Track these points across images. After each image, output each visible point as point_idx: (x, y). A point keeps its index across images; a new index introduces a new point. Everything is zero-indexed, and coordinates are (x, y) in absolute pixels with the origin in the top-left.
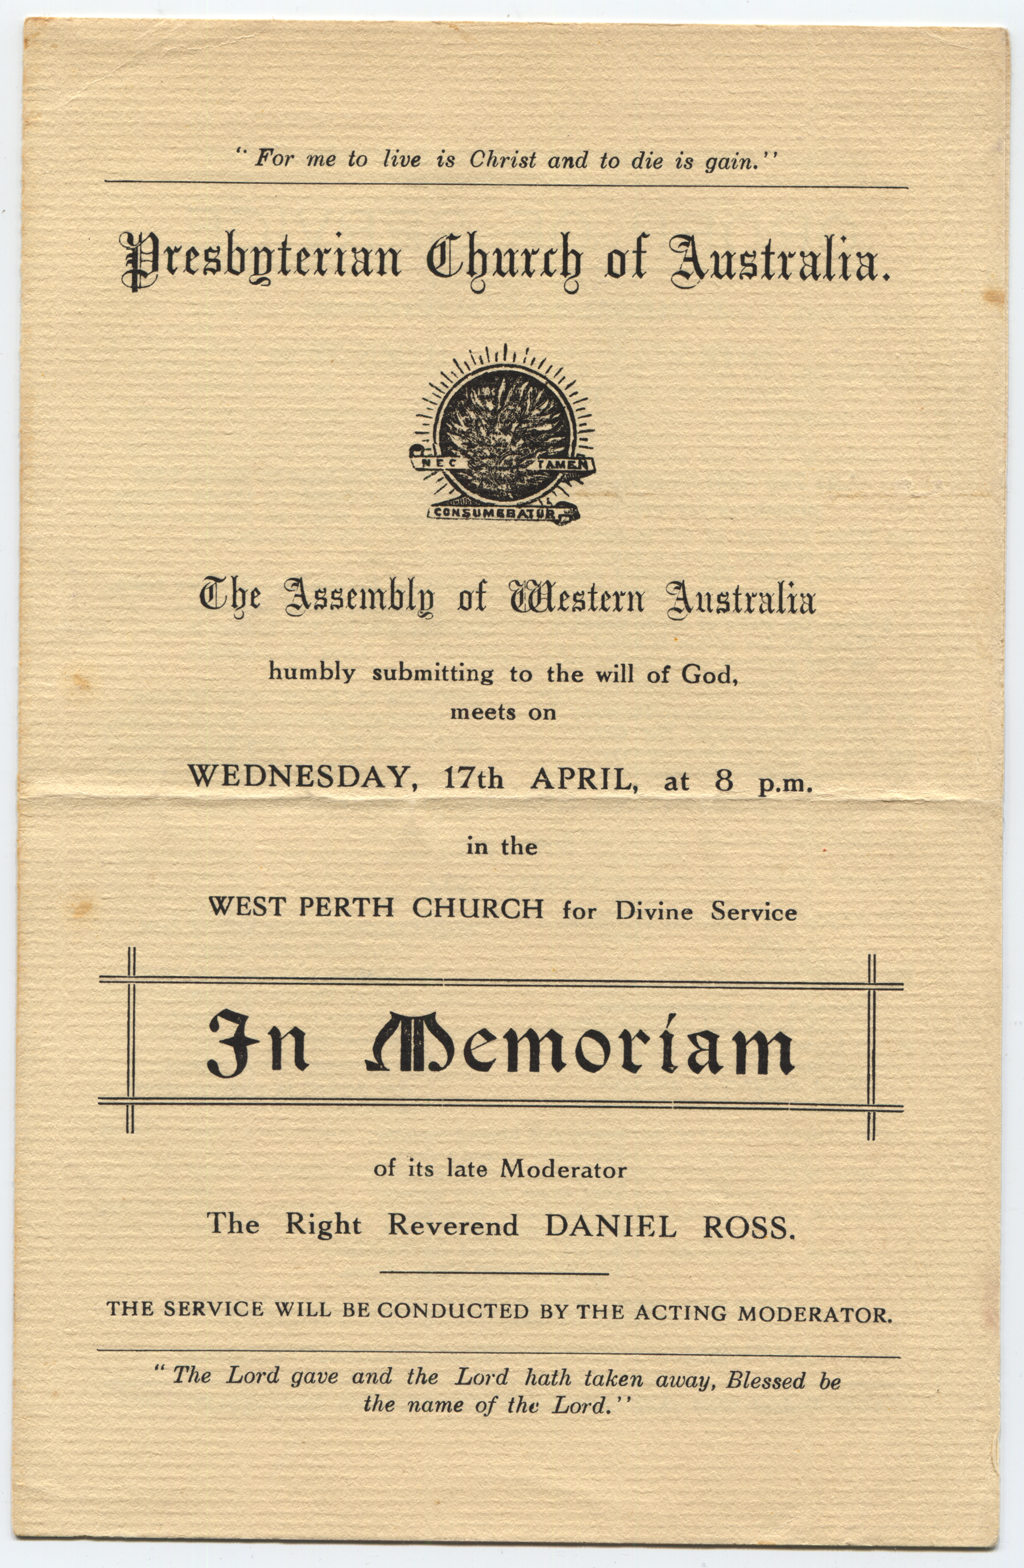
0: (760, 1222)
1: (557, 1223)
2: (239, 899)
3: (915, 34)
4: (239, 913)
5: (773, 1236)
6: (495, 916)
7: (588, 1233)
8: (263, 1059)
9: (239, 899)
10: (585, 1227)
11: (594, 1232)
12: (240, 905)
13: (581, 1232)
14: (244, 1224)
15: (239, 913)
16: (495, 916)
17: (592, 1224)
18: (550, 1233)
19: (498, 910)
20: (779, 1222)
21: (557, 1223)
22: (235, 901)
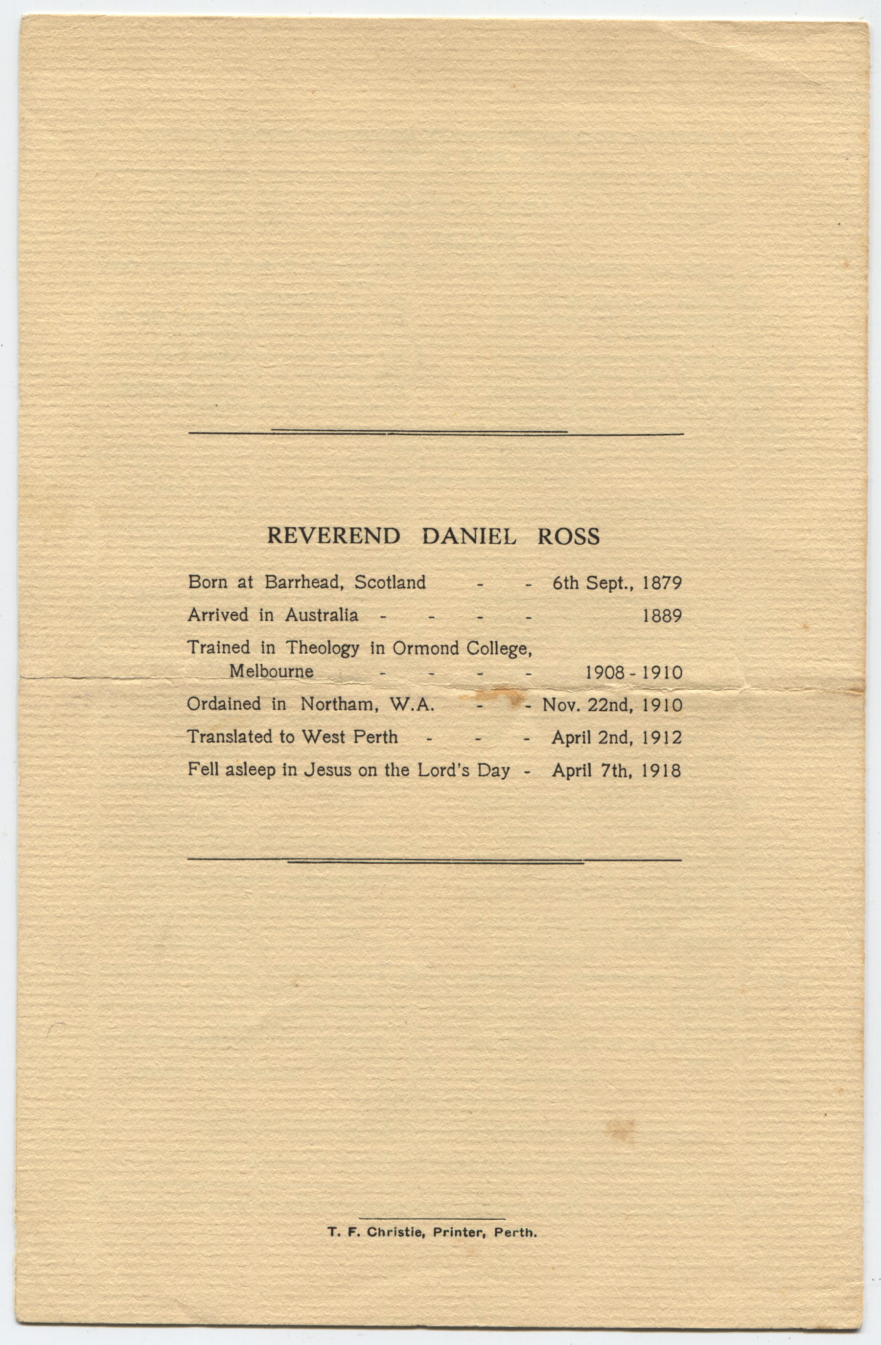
0: (580, 532)
1: (431, 535)
2: (321, 529)
3: (517, 29)
4: (320, 542)
5: (584, 530)
6: (549, 543)
7: (455, 542)
8: (262, 534)
9: (321, 529)
10: (453, 537)
11: (460, 541)
12: (321, 535)
13: (450, 541)
14: (242, 703)
15: (320, 542)
16: (549, 543)
17: (458, 535)
18: (426, 542)
19: (552, 537)
20: (594, 532)
21: (431, 535)
22: (317, 531)
